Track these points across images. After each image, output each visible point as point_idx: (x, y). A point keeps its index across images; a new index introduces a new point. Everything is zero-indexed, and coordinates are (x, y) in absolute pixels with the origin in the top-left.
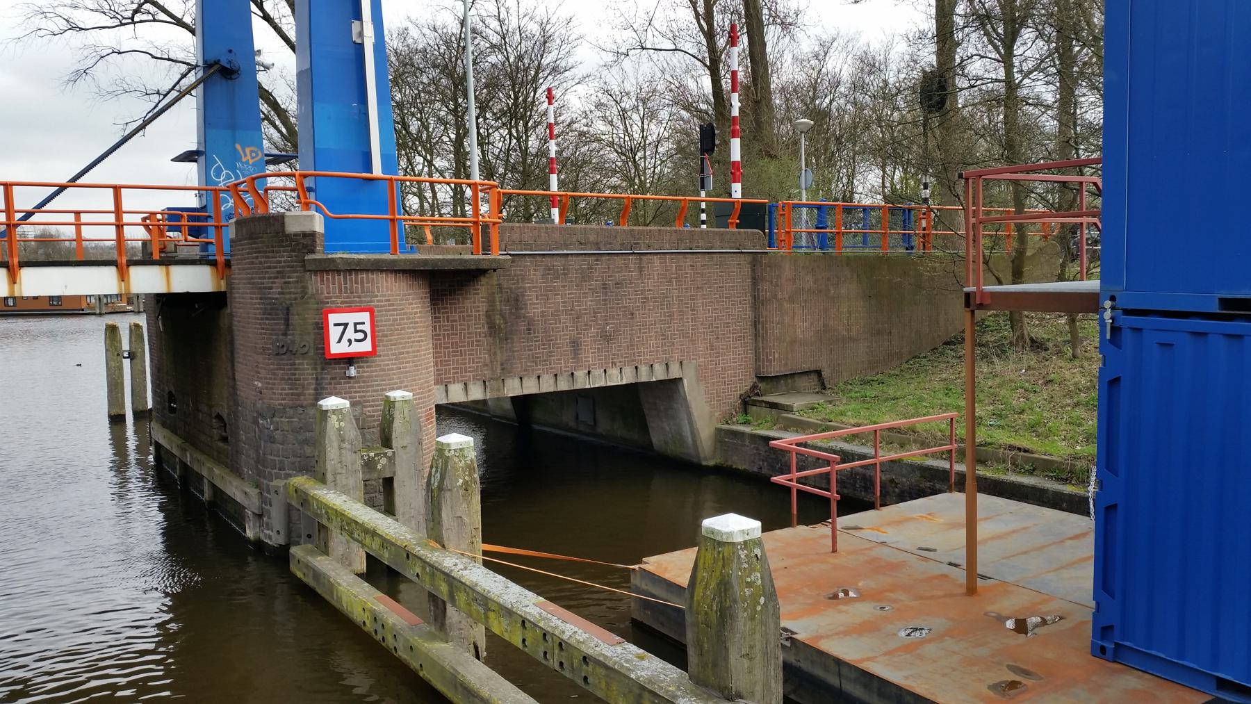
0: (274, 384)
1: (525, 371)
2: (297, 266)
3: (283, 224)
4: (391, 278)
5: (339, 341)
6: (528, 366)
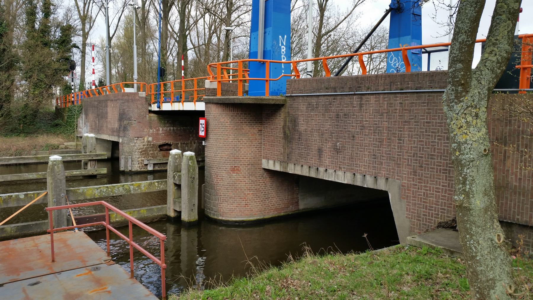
4: (215, 106)
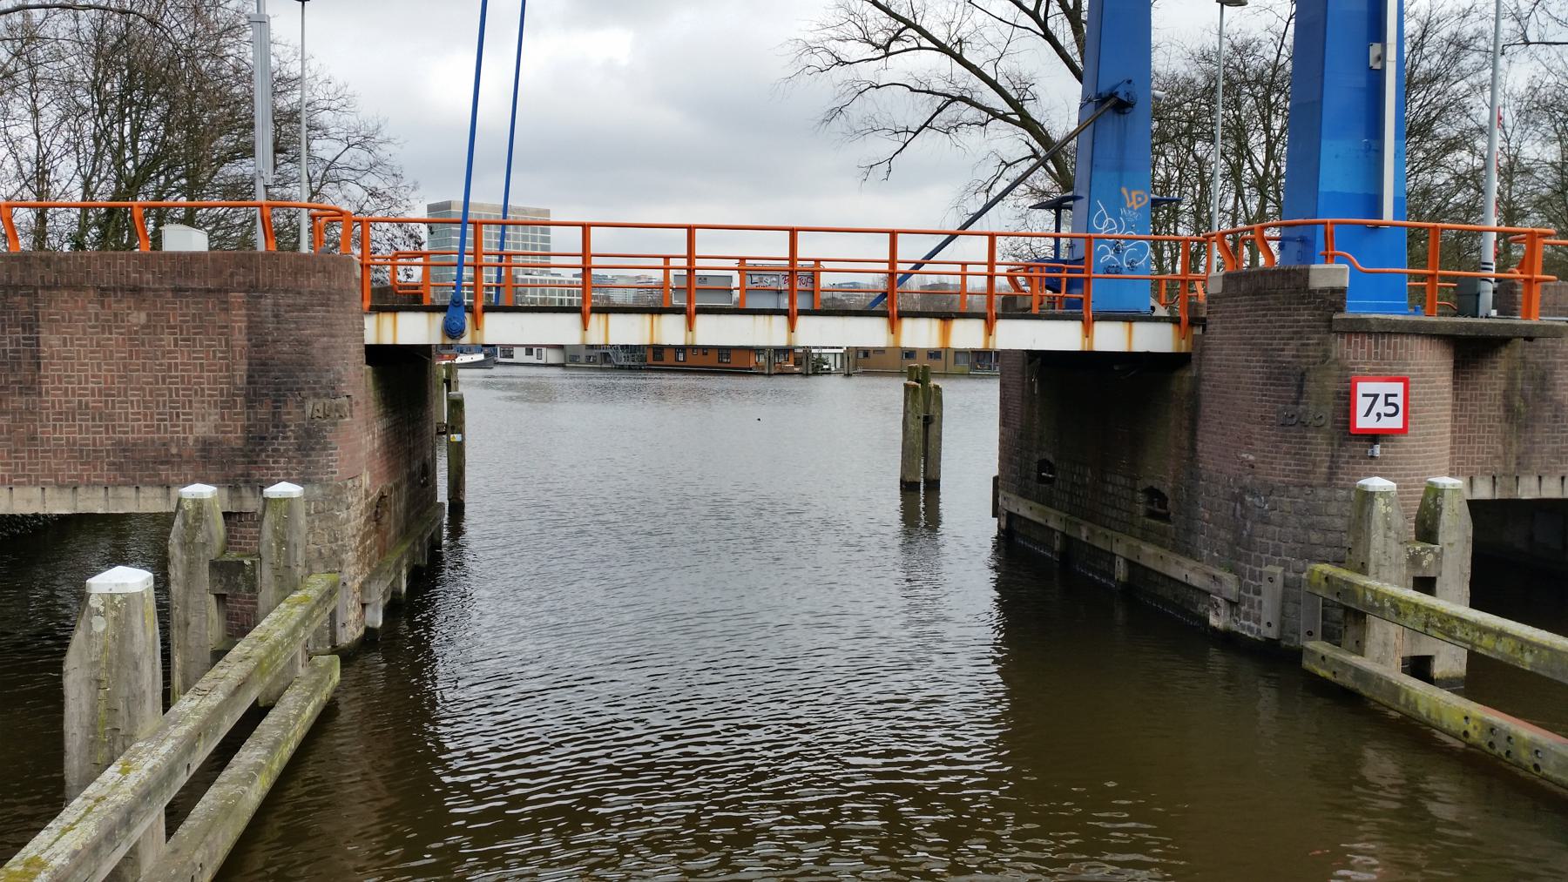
0: (1276, 458)
1: (1547, 468)
2: (1320, 326)
3: (1307, 279)
4: (1426, 342)
5: (1367, 415)
6: (1551, 463)
